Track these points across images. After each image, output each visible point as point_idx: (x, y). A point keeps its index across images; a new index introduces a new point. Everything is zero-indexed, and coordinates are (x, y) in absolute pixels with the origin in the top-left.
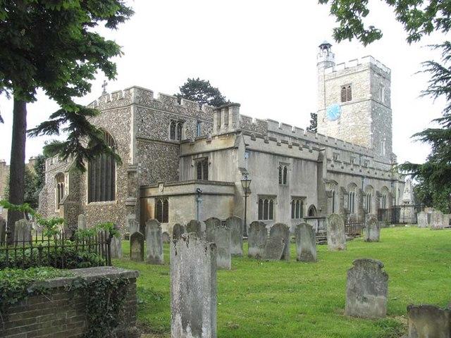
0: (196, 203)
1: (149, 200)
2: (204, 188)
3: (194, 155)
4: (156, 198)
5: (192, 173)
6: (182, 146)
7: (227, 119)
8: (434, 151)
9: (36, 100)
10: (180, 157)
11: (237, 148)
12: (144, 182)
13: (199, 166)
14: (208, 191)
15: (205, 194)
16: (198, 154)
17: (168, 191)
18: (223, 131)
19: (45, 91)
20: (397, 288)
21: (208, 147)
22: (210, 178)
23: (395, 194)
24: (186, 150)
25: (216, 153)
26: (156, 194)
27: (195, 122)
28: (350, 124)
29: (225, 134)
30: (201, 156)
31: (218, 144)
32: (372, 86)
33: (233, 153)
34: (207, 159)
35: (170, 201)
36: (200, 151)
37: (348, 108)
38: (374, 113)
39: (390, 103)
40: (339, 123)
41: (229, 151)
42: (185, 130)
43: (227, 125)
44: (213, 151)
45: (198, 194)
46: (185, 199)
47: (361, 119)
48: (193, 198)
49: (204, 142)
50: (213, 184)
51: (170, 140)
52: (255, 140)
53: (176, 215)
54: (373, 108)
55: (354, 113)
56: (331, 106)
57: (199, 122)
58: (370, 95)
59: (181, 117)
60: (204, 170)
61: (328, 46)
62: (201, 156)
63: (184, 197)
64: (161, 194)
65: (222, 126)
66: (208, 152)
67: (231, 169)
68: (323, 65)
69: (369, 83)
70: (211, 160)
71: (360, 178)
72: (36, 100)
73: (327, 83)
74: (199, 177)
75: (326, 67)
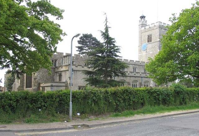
2: (54, 84)
9: (83, 34)
14: (56, 85)
15: (55, 86)
16: (59, 72)
18: (65, 64)
21: (62, 70)
24: (56, 70)
28: (151, 52)
31: (64, 69)
37: (150, 45)
44: (63, 71)
48: (50, 87)
52: (77, 67)
55: (152, 47)
59: (56, 58)
66: (62, 71)
69: (158, 34)
70: (62, 74)
72: (83, 34)
73: (142, 34)
75: (142, 27)
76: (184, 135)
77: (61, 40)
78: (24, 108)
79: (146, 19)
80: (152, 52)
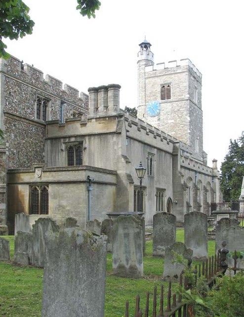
0: (87, 192)
1: (20, 187)
3: (65, 138)
4: (31, 184)
5: (62, 159)
6: (49, 127)
7: (106, 101)
8: (231, 152)
10: (46, 139)
11: (120, 133)
12: (12, 166)
13: (70, 150)
15: (95, 183)
16: (70, 137)
17: (48, 177)
18: (101, 112)
19: (8, 38)
20: (39, 263)
22: (86, 161)
23: (215, 189)
24: (54, 132)
25: (92, 138)
26: (32, 181)
27: (58, 102)
29: (104, 118)
30: (73, 139)
31: (94, 127)
32: (189, 87)
33: (115, 138)
34: (81, 143)
35: (51, 189)
36: (73, 134)
37: (167, 106)
38: (191, 113)
39: (201, 105)
40: (159, 120)
41: (110, 136)
42: (50, 109)
43: (106, 107)
44: (90, 135)
45: (89, 182)
46: (72, 187)
47: (179, 117)
48: (83, 187)
49: (78, 125)
50: (101, 172)
51: (36, 119)
53: (60, 206)
54: (190, 107)
55: (173, 111)
56: (152, 103)
57: (62, 103)
58: (188, 96)
60: (77, 156)
61: (148, 46)
62: (73, 139)
63: (71, 186)
64: (39, 180)
65: (101, 108)
66: (83, 136)
67: (112, 156)
68: (144, 63)
70: (86, 144)
71: (194, 173)
73: (147, 81)
74: (70, 163)
75: (146, 65)
76: (118, 316)
77: (89, 18)
78: (212, 307)
79: (152, 49)
80: (173, 121)
